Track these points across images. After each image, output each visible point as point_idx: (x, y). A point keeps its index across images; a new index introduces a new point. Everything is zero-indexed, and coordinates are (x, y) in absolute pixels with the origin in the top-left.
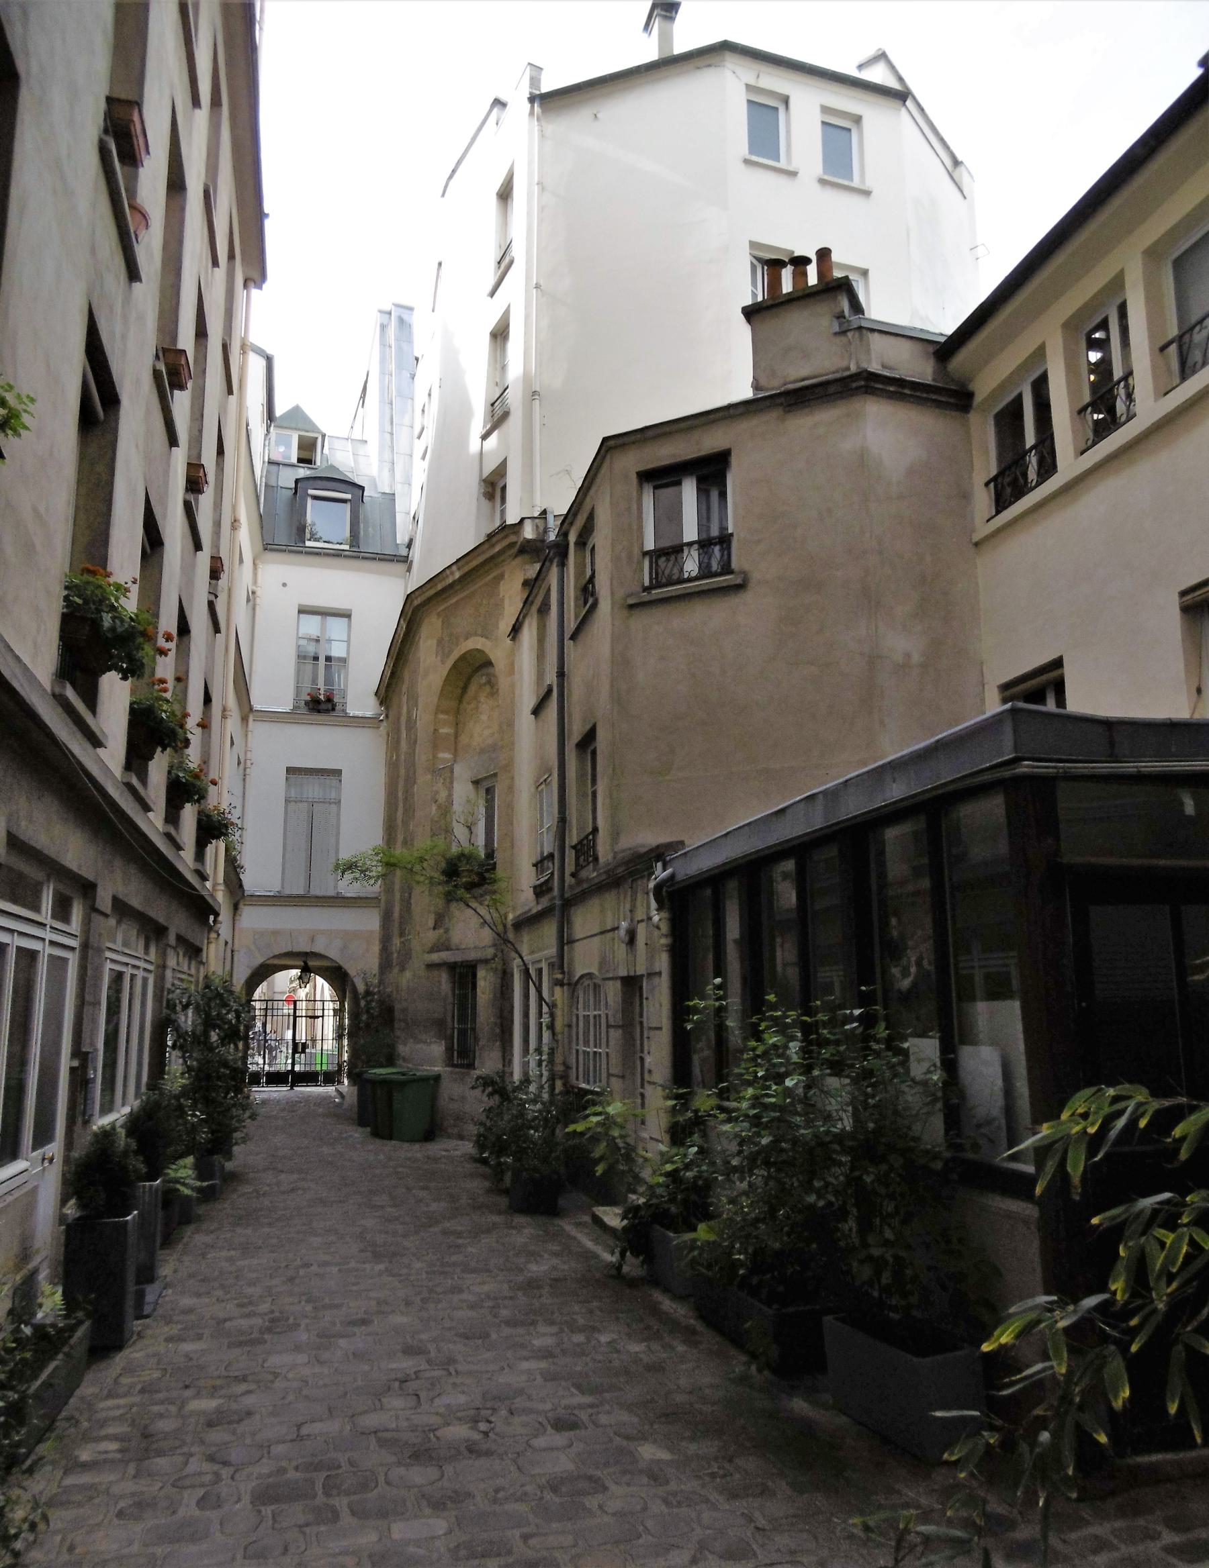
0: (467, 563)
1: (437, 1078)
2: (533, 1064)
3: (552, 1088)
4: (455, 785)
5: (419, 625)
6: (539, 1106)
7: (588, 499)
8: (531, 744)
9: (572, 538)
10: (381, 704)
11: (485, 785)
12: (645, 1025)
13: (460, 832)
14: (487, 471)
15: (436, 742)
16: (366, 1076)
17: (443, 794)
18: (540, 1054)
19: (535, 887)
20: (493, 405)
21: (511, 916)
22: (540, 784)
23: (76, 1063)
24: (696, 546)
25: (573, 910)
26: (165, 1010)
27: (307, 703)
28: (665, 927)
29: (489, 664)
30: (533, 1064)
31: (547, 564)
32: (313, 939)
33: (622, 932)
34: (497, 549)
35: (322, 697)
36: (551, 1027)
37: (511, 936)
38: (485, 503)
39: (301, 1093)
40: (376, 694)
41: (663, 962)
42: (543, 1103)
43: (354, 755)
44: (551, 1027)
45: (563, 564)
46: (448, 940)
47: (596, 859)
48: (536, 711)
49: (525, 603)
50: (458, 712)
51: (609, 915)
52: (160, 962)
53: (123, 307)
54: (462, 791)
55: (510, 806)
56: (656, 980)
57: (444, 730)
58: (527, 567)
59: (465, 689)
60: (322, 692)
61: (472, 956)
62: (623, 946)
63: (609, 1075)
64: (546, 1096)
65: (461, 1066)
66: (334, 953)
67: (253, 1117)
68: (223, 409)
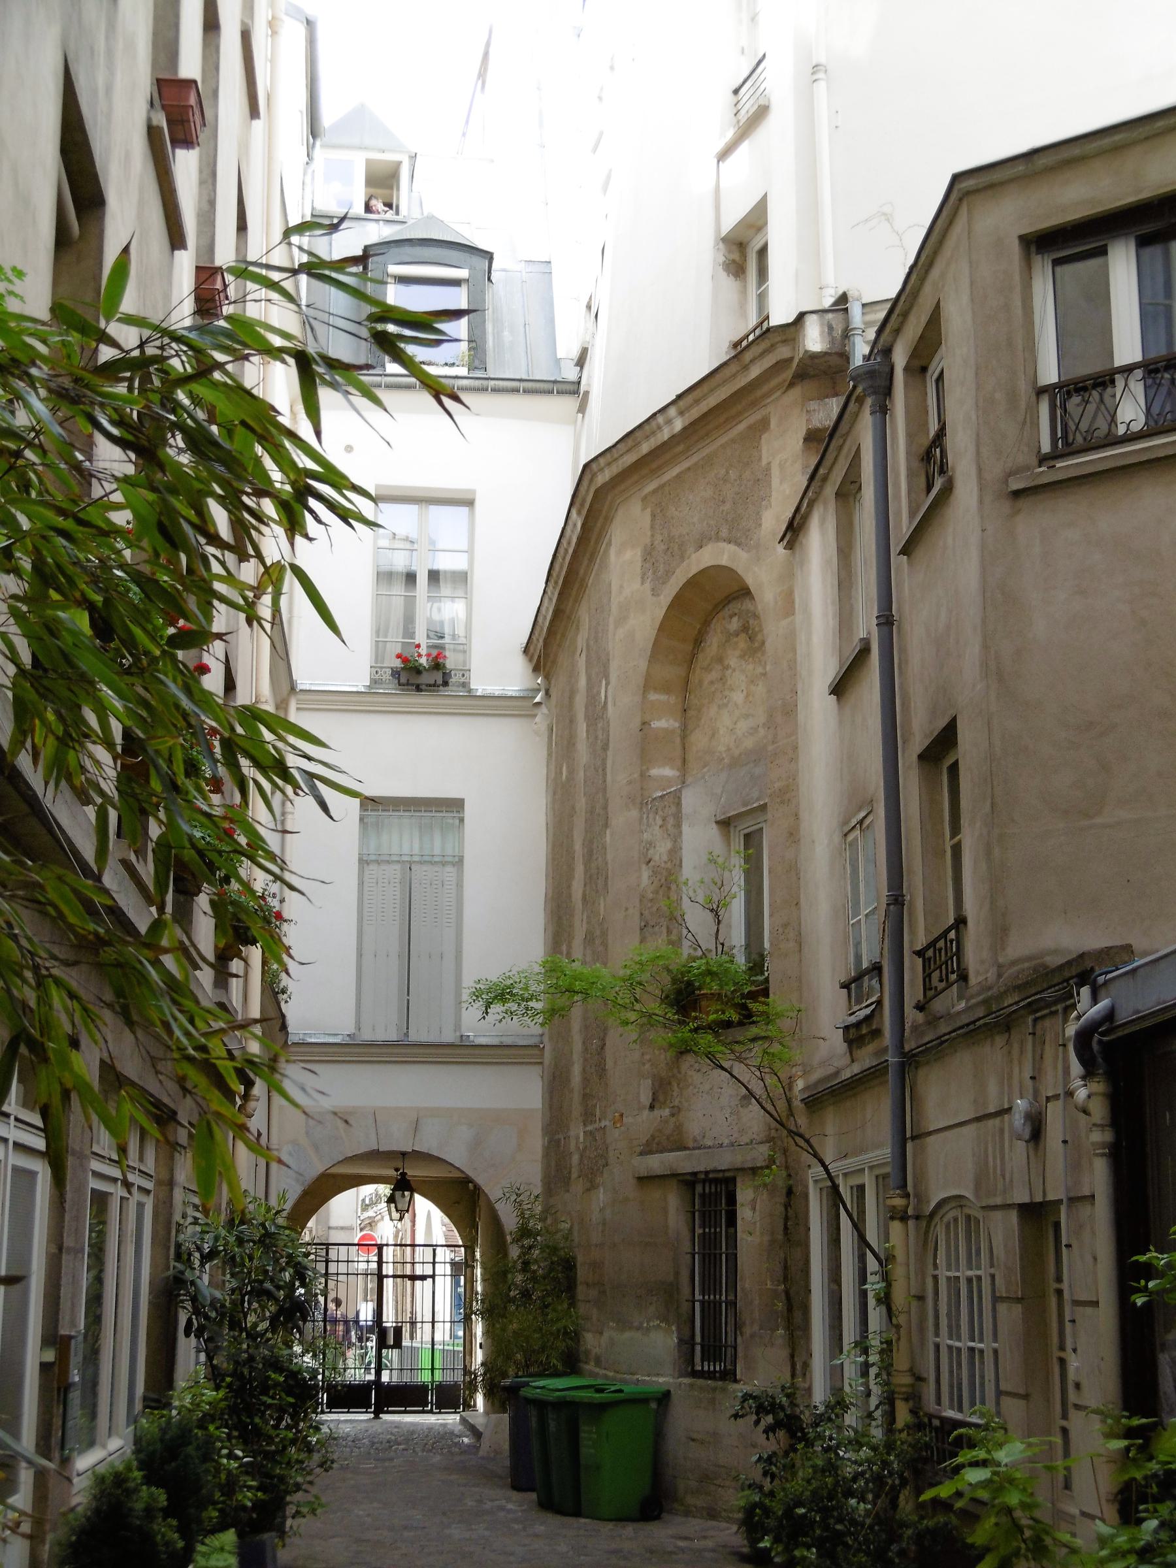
0: (697, 402)
1: (664, 1398)
2: (850, 1371)
3: (891, 1416)
4: (685, 828)
5: (609, 520)
6: (865, 1452)
7: (927, 288)
8: (830, 752)
9: (900, 359)
10: (536, 669)
11: (743, 828)
12: (1066, 1295)
13: (697, 920)
14: (730, 221)
15: (647, 746)
16: (524, 1392)
17: (661, 850)
18: (865, 1351)
19: (846, 1029)
20: (736, 92)
21: (800, 1084)
22: (852, 828)
23: (50, 1356)
24: (1139, 373)
25: (922, 1072)
26: (172, 1263)
27: (395, 673)
28: (1099, 1111)
29: (745, 592)
30: (850, 1371)
31: (852, 406)
32: (416, 1127)
33: (1018, 1120)
34: (755, 372)
35: (423, 661)
36: (885, 1300)
37: (802, 1121)
38: (728, 283)
39: (398, 1425)
40: (526, 651)
41: (1098, 1178)
42: (874, 1448)
43: (486, 772)
44: (885, 1300)
45: (883, 410)
46: (679, 1128)
47: (964, 977)
48: (839, 689)
49: (812, 478)
50: (685, 687)
51: (993, 1088)
52: (164, 1175)
53: (107, 38)
54: (699, 840)
55: (793, 872)
56: (1085, 1210)
57: (660, 724)
58: (813, 405)
59: (698, 642)
60: (423, 651)
61: (724, 1161)
62: (1021, 1146)
63: (999, 1393)
64: (877, 1433)
65: (710, 1375)
66: (458, 1155)
67: (325, 1465)
68: (244, 147)
